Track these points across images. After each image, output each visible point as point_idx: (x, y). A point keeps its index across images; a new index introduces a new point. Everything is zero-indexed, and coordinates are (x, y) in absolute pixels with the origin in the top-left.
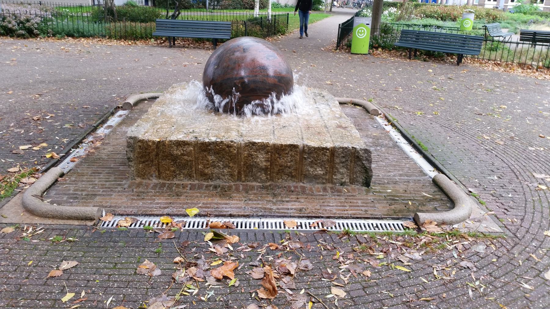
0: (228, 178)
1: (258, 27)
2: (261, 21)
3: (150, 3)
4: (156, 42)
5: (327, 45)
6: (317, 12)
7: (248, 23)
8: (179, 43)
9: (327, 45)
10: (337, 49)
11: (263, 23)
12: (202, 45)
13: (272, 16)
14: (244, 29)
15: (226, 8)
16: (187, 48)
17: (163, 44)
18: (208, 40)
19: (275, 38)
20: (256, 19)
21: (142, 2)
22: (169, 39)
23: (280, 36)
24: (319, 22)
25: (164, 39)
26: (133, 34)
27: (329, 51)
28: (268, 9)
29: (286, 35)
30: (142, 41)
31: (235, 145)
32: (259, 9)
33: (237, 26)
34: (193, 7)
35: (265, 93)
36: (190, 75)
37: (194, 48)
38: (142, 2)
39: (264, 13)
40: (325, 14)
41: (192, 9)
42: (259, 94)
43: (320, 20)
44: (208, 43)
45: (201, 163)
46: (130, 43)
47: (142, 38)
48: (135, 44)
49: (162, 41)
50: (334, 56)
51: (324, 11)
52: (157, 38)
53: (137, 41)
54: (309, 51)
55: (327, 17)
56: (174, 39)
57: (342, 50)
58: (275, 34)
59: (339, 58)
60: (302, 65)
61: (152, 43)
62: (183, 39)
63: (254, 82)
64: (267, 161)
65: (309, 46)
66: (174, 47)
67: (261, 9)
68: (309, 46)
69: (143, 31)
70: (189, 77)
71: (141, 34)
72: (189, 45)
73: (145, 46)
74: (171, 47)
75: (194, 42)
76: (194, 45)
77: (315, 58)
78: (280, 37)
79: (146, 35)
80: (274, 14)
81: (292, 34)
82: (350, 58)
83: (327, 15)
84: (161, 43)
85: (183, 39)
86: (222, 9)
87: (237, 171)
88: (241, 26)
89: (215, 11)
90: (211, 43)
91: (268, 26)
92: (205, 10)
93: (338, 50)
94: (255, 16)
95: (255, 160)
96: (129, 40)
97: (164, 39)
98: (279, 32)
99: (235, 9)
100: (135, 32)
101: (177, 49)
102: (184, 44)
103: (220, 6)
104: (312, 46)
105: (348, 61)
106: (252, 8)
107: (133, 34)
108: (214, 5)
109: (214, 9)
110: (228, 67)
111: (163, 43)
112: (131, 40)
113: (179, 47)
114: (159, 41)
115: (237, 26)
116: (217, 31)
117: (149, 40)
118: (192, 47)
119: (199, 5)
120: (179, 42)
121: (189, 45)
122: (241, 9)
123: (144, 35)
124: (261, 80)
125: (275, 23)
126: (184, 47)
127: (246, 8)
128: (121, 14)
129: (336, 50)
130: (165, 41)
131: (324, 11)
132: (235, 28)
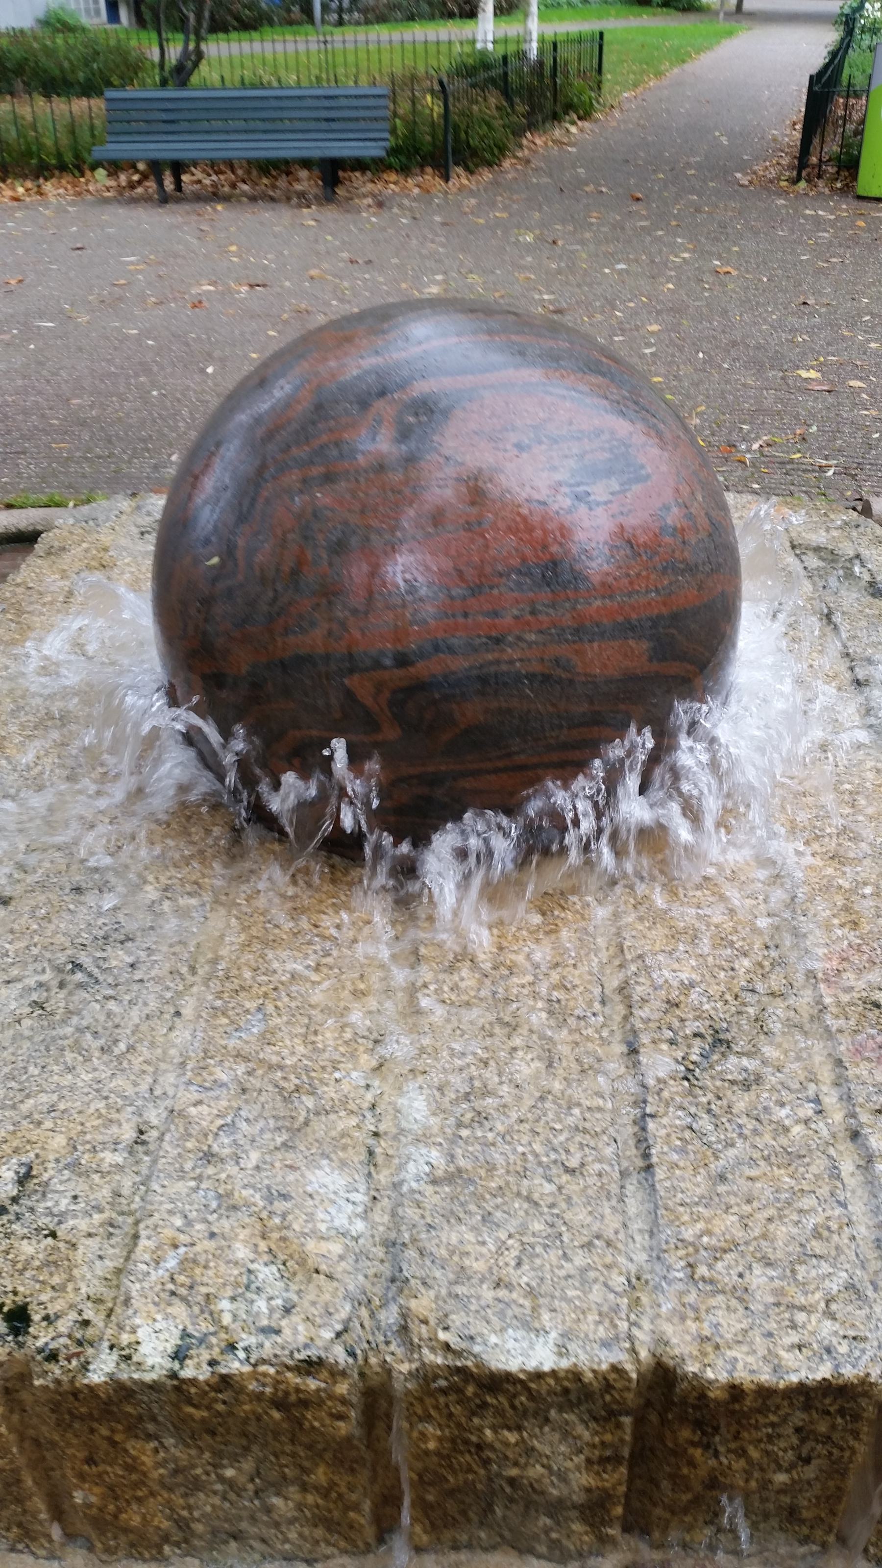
0: (301, 1535)
1: (494, 99)
2: (506, 74)
3: (124, 14)
4: (112, 183)
5: (757, 158)
6: (692, 17)
7: (458, 85)
8: (199, 182)
9: (757, 158)
10: (799, 179)
11: (512, 77)
12: (282, 182)
13: (542, 41)
14: (438, 110)
15: (382, 19)
16: (226, 199)
17: (140, 190)
18: (306, 163)
19: (557, 133)
20: (483, 63)
21: (98, 12)
22: (155, 168)
23: (573, 123)
24: (706, 59)
25: (141, 166)
26: (29, 154)
27: (768, 186)
28: (526, 15)
29: (597, 121)
30: (64, 182)
31: (342, 1388)
32: (495, 14)
33: (414, 101)
34: (271, 23)
35: (565, 746)
36: (209, 358)
37: (253, 199)
38: (98, 12)
39: (511, 28)
40: (722, 25)
41: (267, 29)
42: (521, 759)
43: (709, 48)
44: (303, 174)
45: (82, 1477)
46: (21, 190)
47: (63, 168)
48: (40, 193)
49: (136, 178)
50: (796, 211)
51: (717, 13)
52: (114, 167)
53: (46, 179)
54: (693, 191)
55: (730, 34)
56: (178, 168)
57: (821, 183)
58: (556, 117)
59: (818, 222)
60: (678, 268)
61: (99, 186)
62: (214, 166)
63: (484, 680)
64: (603, 1461)
65: (688, 165)
66: (178, 201)
67: (502, 13)
68: (688, 165)
69: (65, 140)
70: (203, 371)
71: (59, 155)
72: (233, 186)
73: (73, 204)
74: (164, 199)
75: (255, 173)
76: (255, 184)
77: (723, 226)
78: (573, 129)
79: (77, 156)
80: (549, 34)
81: (617, 114)
82: (861, 223)
83: (727, 26)
84: (132, 186)
85: (214, 166)
86: (368, 22)
87: (367, 1506)
88: (429, 98)
89: (345, 29)
90: (316, 172)
91: (531, 90)
92: (309, 28)
93: (803, 184)
94: (479, 46)
95: (514, 1472)
96: (17, 176)
97: (141, 166)
98: (569, 107)
99: (411, 18)
100: (34, 148)
101: (187, 207)
102: (214, 185)
103: (359, 11)
104: (699, 167)
105: (855, 240)
106: (471, 13)
107: (29, 154)
108: (340, 10)
109: (340, 23)
110: (295, 573)
111: (139, 182)
112: (25, 177)
113: (198, 198)
114: (123, 178)
115: (414, 101)
116: (334, 126)
117: (88, 173)
118: (244, 194)
119: (289, 11)
120: (199, 175)
121: (233, 186)
122: (432, 18)
123: (69, 157)
124: (536, 667)
125: (554, 75)
126: (215, 196)
127: (451, 15)
128: (8, 65)
129: (795, 181)
130: (145, 177)
131: (717, 13)
132: (404, 107)
